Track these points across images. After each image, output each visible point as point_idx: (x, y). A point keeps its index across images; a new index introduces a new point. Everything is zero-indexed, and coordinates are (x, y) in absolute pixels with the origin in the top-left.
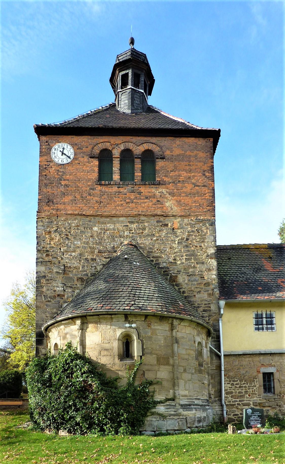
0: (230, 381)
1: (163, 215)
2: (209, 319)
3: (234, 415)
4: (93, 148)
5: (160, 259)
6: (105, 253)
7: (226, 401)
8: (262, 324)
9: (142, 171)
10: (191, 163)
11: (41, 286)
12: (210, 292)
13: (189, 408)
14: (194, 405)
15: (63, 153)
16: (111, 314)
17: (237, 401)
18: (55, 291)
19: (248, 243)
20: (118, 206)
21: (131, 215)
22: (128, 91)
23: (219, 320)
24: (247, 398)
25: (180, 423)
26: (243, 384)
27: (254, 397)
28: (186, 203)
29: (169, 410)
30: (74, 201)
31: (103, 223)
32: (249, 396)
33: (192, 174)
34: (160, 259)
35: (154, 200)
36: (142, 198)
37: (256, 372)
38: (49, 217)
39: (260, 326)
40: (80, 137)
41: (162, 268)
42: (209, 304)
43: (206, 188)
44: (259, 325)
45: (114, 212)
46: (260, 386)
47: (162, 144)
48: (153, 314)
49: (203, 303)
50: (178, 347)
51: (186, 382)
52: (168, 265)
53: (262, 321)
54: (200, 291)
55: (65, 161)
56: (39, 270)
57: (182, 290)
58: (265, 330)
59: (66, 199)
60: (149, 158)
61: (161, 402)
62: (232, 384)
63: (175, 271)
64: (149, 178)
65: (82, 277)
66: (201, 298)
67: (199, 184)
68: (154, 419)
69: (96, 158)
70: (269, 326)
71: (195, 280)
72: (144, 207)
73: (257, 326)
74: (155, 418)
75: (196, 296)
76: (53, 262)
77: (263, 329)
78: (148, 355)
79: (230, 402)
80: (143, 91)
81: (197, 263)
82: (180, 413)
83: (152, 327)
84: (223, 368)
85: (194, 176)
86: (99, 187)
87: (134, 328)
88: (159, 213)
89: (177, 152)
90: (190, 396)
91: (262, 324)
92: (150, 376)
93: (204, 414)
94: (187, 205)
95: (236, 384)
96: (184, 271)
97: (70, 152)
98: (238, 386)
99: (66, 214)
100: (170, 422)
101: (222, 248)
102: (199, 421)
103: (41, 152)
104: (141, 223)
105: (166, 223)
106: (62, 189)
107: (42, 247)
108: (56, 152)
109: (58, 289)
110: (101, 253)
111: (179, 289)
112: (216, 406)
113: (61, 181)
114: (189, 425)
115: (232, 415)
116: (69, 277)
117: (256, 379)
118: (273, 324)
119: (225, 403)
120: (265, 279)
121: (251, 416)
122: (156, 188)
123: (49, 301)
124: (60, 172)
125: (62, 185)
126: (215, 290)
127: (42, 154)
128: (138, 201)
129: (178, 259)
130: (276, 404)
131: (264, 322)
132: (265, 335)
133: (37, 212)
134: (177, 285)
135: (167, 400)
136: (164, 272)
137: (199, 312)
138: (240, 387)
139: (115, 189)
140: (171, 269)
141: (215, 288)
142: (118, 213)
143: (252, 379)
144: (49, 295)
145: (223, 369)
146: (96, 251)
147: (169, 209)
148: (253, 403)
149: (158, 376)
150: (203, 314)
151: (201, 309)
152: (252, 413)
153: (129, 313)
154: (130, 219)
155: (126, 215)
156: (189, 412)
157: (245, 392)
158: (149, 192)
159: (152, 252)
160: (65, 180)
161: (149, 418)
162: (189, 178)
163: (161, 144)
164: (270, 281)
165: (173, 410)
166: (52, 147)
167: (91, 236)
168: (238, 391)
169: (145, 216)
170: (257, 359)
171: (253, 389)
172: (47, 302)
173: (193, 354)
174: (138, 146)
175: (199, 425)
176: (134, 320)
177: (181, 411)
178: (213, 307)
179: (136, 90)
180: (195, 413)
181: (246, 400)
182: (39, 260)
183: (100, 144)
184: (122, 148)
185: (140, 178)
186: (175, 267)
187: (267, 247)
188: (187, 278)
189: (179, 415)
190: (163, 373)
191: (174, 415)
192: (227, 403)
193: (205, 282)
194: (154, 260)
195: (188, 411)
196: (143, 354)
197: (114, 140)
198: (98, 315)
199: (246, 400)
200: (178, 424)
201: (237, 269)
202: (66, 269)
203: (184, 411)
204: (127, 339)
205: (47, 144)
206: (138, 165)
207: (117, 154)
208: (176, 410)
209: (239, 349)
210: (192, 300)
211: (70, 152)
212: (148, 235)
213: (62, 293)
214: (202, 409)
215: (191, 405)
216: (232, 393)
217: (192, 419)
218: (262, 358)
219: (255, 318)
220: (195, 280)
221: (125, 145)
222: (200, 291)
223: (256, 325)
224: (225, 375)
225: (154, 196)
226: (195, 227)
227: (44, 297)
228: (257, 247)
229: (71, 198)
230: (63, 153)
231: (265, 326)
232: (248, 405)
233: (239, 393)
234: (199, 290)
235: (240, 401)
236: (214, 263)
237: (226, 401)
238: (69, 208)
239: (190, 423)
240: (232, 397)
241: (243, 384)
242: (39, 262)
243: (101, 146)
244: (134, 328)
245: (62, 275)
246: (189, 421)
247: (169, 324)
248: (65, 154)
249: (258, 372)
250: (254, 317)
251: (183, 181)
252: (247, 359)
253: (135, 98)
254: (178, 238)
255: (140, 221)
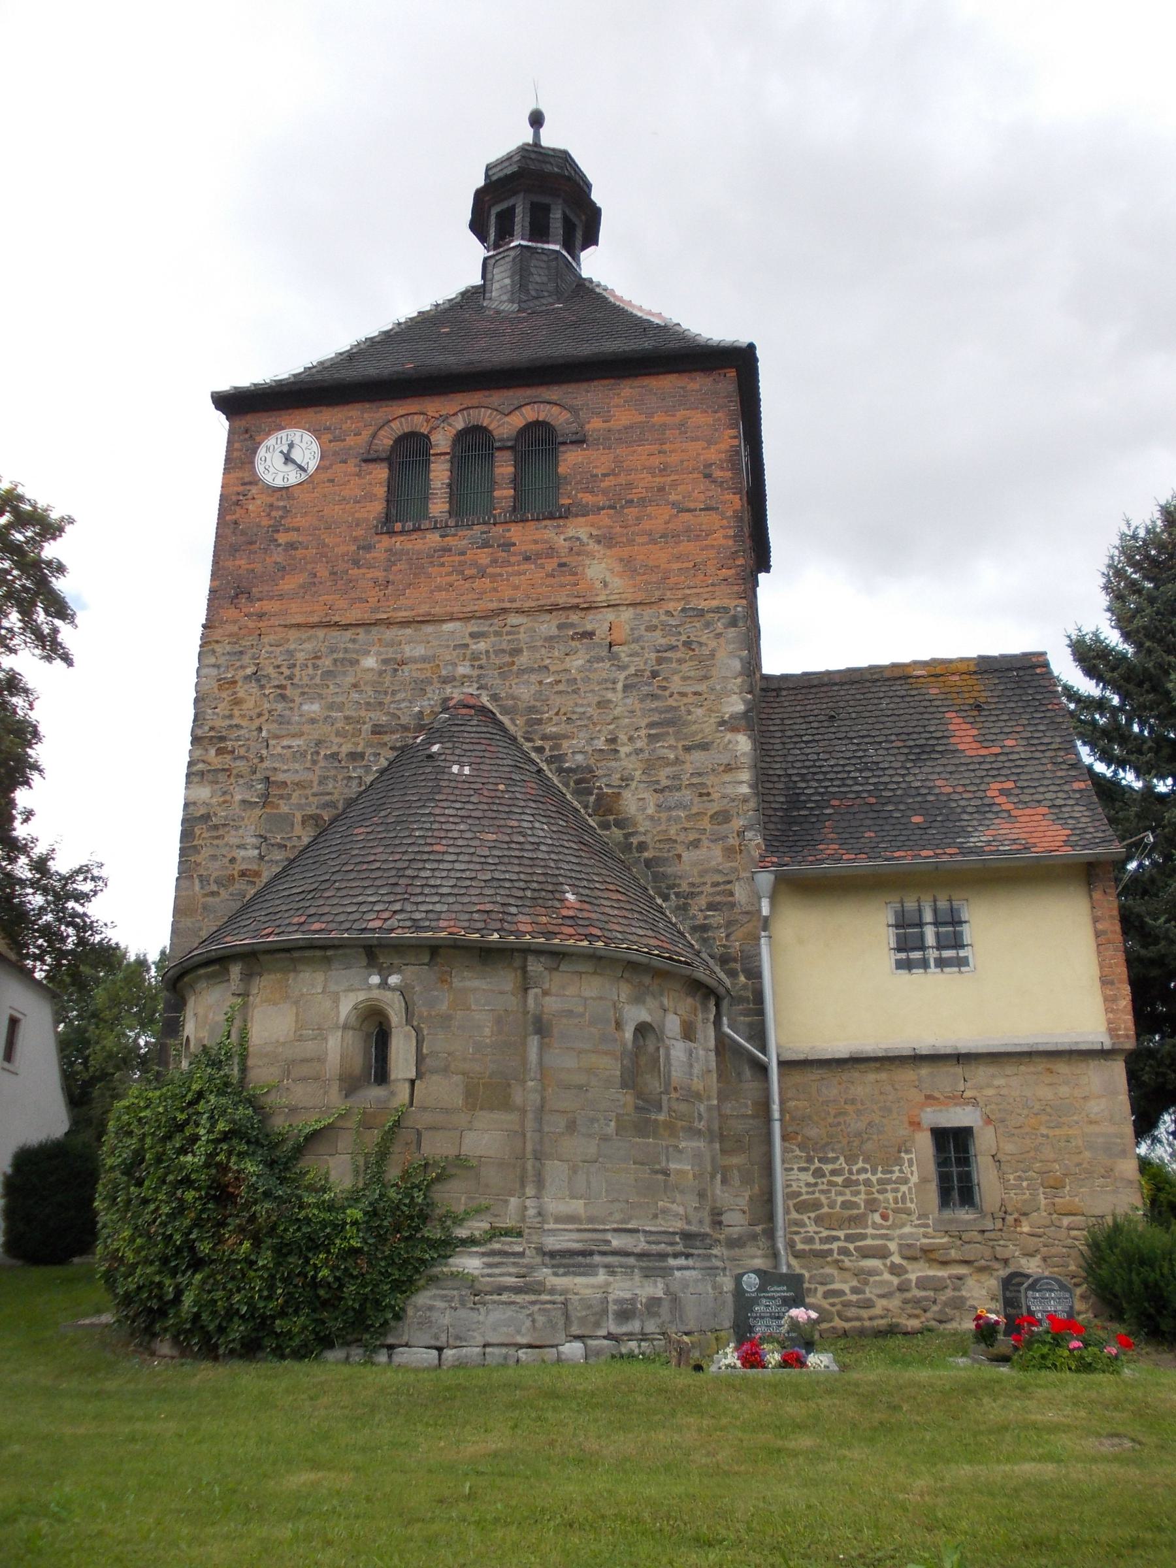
0: (810, 1160)
1: (576, 607)
2: (728, 936)
3: (827, 1295)
4: (374, 436)
5: (565, 744)
6: (392, 732)
7: (796, 1238)
8: (922, 948)
9: (517, 482)
10: (666, 447)
11: (195, 846)
12: (731, 841)
13: (580, 1266)
14: (604, 1253)
15: (288, 459)
16: (324, 948)
17: (837, 1239)
18: (233, 860)
19: (905, 659)
20: (439, 589)
21: (478, 614)
22: (512, 253)
23: (759, 939)
24: (875, 1226)
25: (541, 1320)
26: (859, 1172)
27: (903, 1225)
28: (651, 564)
29: (497, 1271)
30: (311, 586)
31: (391, 644)
32: (884, 1217)
33: (672, 478)
34: (565, 744)
35: (551, 565)
36: (513, 559)
37: (906, 1125)
38: (235, 638)
39: (916, 955)
40: (336, 409)
41: (569, 770)
42: (729, 882)
43: (714, 516)
44: (909, 949)
45: (424, 609)
46: (924, 1180)
47: (578, 402)
48: (452, 943)
49: (709, 879)
50: (542, 1048)
51: (574, 1170)
52: (592, 761)
53: (922, 936)
54: (699, 840)
55: (293, 477)
56: (192, 799)
57: (634, 840)
58: (933, 969)
59: (289, 584)
60: (539, 443)
61: (472, 1241)
62: (818, 1173)
63: (615, 779)
64: (539, 499)
65: (318, 811)
66: (699, 862)
67: (692, 505)
68: (439, 1304)
69: (382, 460)
70: (947, 954)
71: (680, 806)
72: (516, 588)
73: (903, 955)
74: (443, 1298)
75: (685, 855)
76: (234, 772)
77: (924, 964)
78: (435, 1078)
79: (810, 1240)
80: (557, 248)
81: (687, 749)
82: (542, 1283)
83: (457, 983)
84: (776, 1107)
85: (674, 484)
86: (385, 538)
87: (393, 989)
88: (562, 600)
89: (623, 418)
90: (591, 1220)
91: (922, 948)
92: (436, 1147)
93: (656, 1289)
94: (654, 569)
95: (834, 1172)
96: (644, 778)
97: (307, 452)
98: (839, 1180)
99: (286, 626)
100: (497, 1315)
101: (815, 682)
102: (625, 1315)
103: (228, 460)
104: (508, 633)
105: (589, 628)
106: (278, 556)
107: (207, 728)
108: (268, 456)
109: (243, 853)
110: (380, 733)
111: (627, 836)
112: (753, 1257)
113: (276, 536)
114: (575, 1330)
115: (820, 1294)
116: (280, 815)
117: (907, 1152)
118: (962, 946)
119: (791, 1245)
120: (943, 786)
121: (755, 1301)
122: (559, 526)
123: (213, 894)
124: (278, 508)
125: (280, 545)
126: (749, 835)
127: (231, 464)
128: (503, 571)
129: (623, 738)
130: (988, 1253)
131: (930, 940)
132: (931, 984)
133: (204, 626)
134: (619, 824)
135: (496, 1233)
136: (578, 782)
137: (694, 910)
138: (848, 1183)
139: (434, 538)
140: (599, 773)
141: (746, 828)
142: (437, 610)
143: (892, 1155)
144: (214, 875)
145: (776, 1115)
146: (367, 727)
147: (599, 585)
148: (900, 1245)
149: (465, 1150)
150: (706, 918)
151: (702, 901)
152: (762, 1288)
153: (375, 942)
154: (473, 627)
155: (461, 616)
156: (579, 1280)
157: (867, 1202)
158: (536, 542)
159: (539, 722)
160: (287, 530)
161: (422, 1299)
162: (661, 489)
163: (575, 402)
164: (960, 789)
165: (512, 1270)
166: (260, 444)
167: (355, 686)
168: (840, 1199)
169: (520, 611)
170: (908, 1075)
171: (896, 1190)
172: (206, 895)
173: (611, 1067)
174: (505, 415)
175: (625, 1329)
176: (396, 962)
177: (545, 1275)
178: (740, 893)
179: (536, 248)
180: (608, 1284)
181: (874, 1237)
182: (195, 769)
183: (397, 422)
184: (459, 424)
185: (508, 504)
186: (613, 764)
187: (972, 668)
188: (651, 800)
189: (536, 1288)
190: (484, 1138)
191: (517, 1290)
192: (800, 1246)
193: (715, 807)
194: (547, 745)
195: (575, 1274)
196: (420, 1075)
197: (434, 406)
198: (288, 950)
199: (874, 1237)
200: (528, 1323)
201: (849, 754)
202: (274, 791)
203: (556, 1274)
204: (381, 1024)
205: (247, 436)
206: (504, 467)
207: (443, 443)
208: (523, 1271)
209: (840, 1045)
210: (669, 870)
211: (307, 452)
212: (531, 670)
213: (255, 867)
214: (641, 1268)
215: (591, 1253)
216: (817, 1205)
217: (590, 1307)
218: (925, 1071)
219: (897, 926)
220: (680, 806)
221: (469, 415)
222: (699, 840)
223: (899, 949)
224: (784, 1138)
225: (551, 552)
226: (680, 633)
227: (201, 881)
228: (939, 670)
229: (302, 578)
230: (288, 459)
231: (932, 954)
232: (883, 1254)
233: (846, 1205)
234: (692, 836)
235: (849, 1238)
236: (743, 744)
237: (796, 1238)
238: (294, 607)
239: (583, 1321)
240: (818, 1221)
241: (859, 1172)
242: (194, 775)
243: (399, 427)
244: (393, 989)
245: (258, 812)
246: (577, 1313)
247: (515, 969)
248: (294, 462)
249: (915, 1125)
250: (892, 921)
251: (643, 499)
252: (871, 1077)
253: (533, 270)
254: (627, 673)
255: (508, 628)
